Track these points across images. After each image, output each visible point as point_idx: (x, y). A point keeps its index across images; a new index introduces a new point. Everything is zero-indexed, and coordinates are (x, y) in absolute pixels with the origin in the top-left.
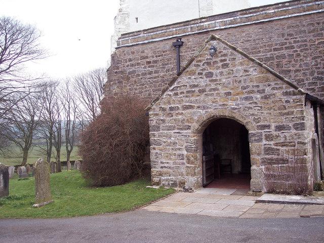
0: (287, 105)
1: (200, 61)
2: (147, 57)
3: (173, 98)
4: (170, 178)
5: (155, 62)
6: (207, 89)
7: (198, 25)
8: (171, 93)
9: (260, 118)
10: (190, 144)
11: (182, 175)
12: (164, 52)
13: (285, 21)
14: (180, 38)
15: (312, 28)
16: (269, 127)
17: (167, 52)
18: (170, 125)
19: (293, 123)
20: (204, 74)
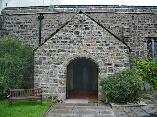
0: (121, 53)
1: (71, 24)
2: (21, 23)
3: (52, 44)
4: (47, 94)
5: (26, 26)
6: (75, 41)
7: (53, 9)
8: (51, 42)
9: (106, 60)
10: (62, 73)
11: (56, 92)
12: (32, 21)
13: (100, 14)
14: (42, 14)
15: (112, 20)
17: (33, 21)
18: (49, 61)
19: (124, 63)
20: (73, 32)
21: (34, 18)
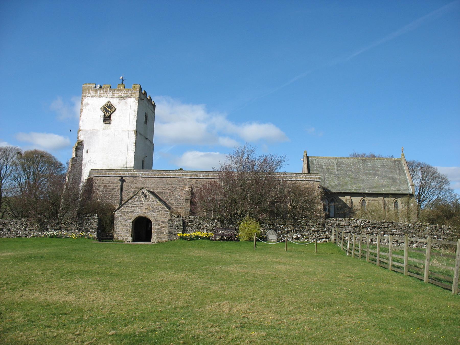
12: (114, 182)
14: (123, 177)
16: (159, 221)
21: (116, 180)
